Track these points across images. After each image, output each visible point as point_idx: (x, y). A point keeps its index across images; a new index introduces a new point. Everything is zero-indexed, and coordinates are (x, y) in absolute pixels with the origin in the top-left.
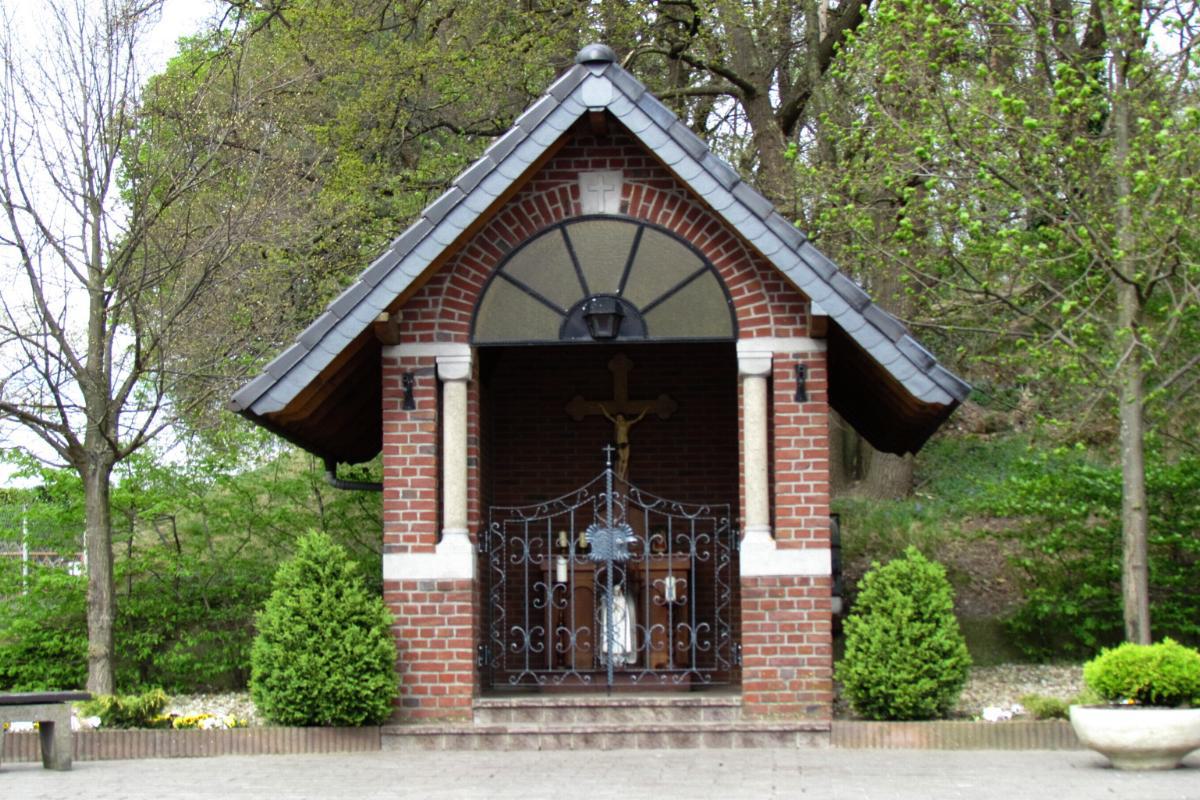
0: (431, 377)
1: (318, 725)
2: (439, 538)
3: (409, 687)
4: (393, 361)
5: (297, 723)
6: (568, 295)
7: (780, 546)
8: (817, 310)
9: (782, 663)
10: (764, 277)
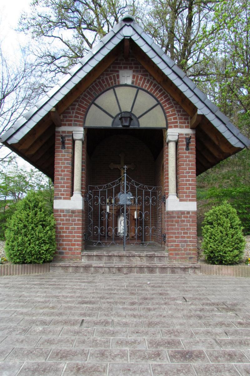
0: (71, 138)
1: (26, 263)
2: (72, 194)
3: (61, 247)
4: (59, 132)
5: (18, 263)
6: (115, 112)
7: (181, 200)
8: (199, 112)
9: (181, 242)
10: (176, 107)
